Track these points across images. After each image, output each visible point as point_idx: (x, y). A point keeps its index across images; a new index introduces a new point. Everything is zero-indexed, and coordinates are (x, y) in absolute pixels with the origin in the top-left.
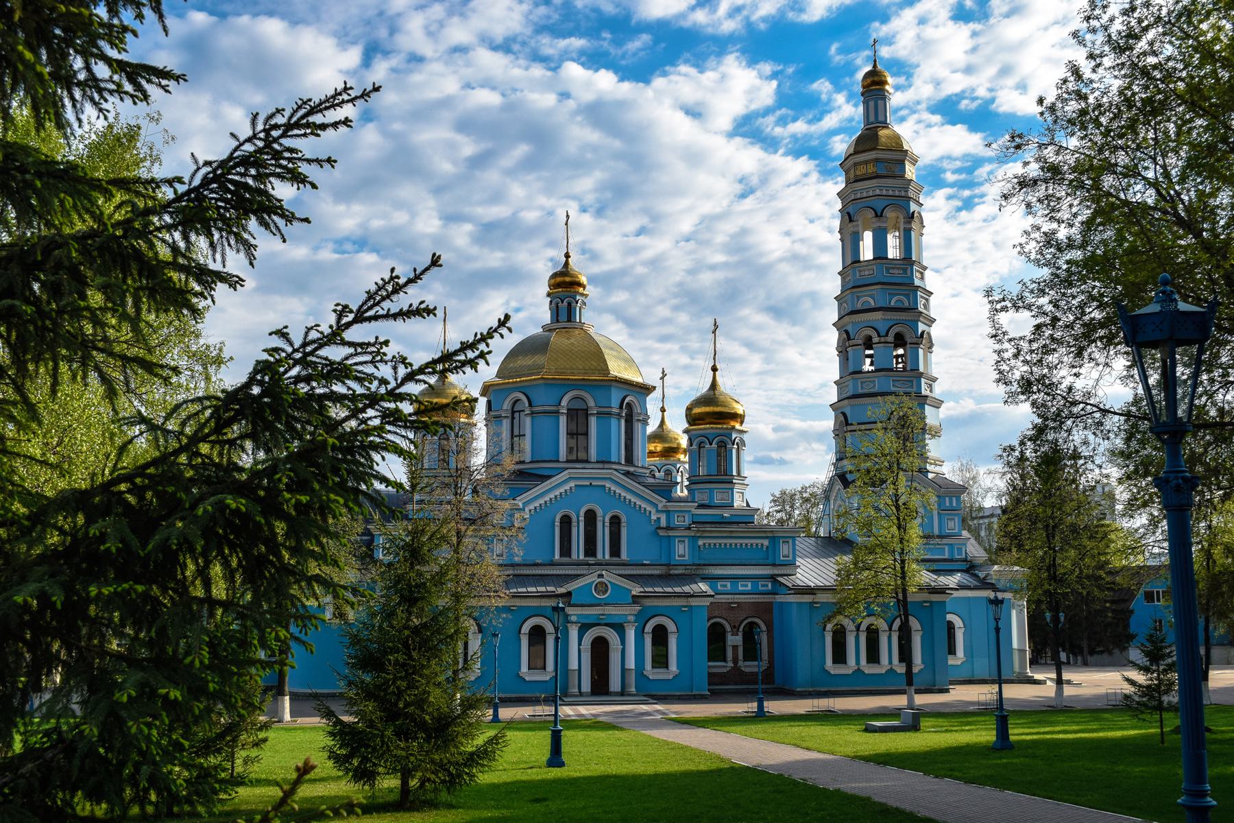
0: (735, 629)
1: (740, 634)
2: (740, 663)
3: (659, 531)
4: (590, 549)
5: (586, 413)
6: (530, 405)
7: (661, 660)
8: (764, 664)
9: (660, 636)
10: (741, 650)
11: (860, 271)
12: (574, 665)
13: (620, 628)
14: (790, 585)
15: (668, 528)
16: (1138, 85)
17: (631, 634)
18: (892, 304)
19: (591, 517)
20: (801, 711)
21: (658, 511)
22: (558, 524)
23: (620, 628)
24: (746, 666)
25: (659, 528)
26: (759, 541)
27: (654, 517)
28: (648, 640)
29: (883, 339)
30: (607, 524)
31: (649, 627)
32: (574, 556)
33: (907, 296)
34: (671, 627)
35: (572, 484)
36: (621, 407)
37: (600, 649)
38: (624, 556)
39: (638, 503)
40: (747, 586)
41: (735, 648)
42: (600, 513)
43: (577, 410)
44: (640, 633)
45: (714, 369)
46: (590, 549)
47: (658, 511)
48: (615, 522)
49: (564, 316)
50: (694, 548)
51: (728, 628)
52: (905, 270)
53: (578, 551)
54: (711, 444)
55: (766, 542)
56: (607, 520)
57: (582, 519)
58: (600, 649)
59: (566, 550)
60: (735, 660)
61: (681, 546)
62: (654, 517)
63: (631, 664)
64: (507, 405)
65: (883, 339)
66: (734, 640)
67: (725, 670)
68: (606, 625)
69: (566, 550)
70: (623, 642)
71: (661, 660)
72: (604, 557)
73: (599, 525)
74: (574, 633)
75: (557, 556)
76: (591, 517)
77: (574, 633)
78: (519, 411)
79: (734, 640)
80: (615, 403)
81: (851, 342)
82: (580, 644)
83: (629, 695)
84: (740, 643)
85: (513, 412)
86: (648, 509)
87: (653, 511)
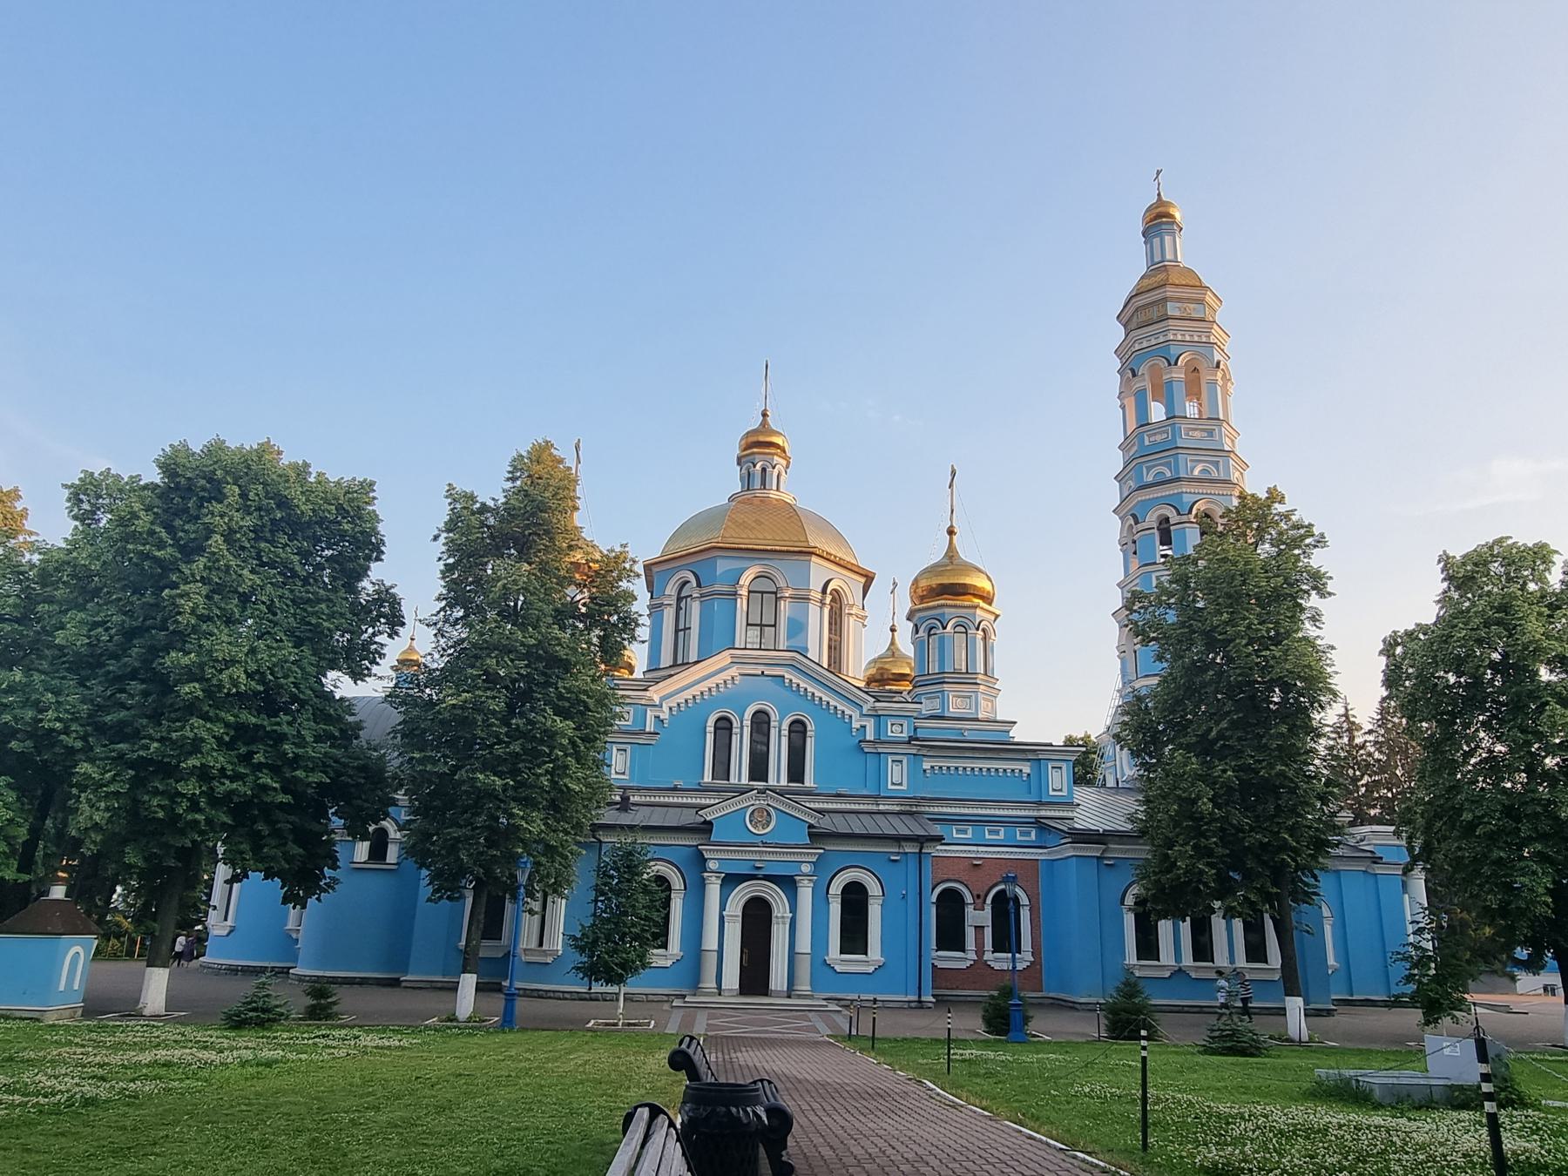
0: (979, 899)
1: (988, 909)
2: (988, 956)
3: (863, 745)
4: (759, 769)
5: (776, 595)
6: (699, 585)
7: (854, 938)
8: (1025, 958)
9: (855, 899)
10: (988, 933)
11: (1149, 436)
12: (711, 942)
13: (788, 883)
14: (1066, 829)
15: (877, 742)
16: (1179, 869)
17: (805, 893)
18: (1196, 472)
19: (761, 722)
20: (1225, 934)
21: (862, 715)
22: (710, 729)
23: (788, 883)
24: (996, 960)
25: (865, 741)
26: (1017, 766)
27: (856, 725)
28: (835, 909)
29: (1185, 518)
30: (785, 733)
31: (836, 888)
32: (733, 780)
33: (1216, 464)
34: (874, 888)
35: (734, 671)
36: (824, 591)
37: (757, 918)
38: (809, 782)
39: (832, 703)
40: (997, 833)
41: (979, 929)
42: (775, 716)
43: (762, 593)
44: (821, 897)
45: (951, 532)
46: (759, 769)
47: (862, 715)
48: (798, 730)
49: (757, 483)
50: (916, 773)
51: (969, 899)
52: (1211, 433)
53: (740, 773)
54: (944, 628)
55: (1026, 769)
56: (785, 726)
57: (747, 723)
58: (757, 918)
59: (722, 767)
60: (980, 951)
61: (897, 768)
62: (856, 725)
63: (804, 944)
64: (671, 589)
65: (1185, 518)
66: (978, 917)
67: (963, 965)
68: (767, 878)
69: (722, 767)
70: (793, 909)
71: (854, 938)
72: (740, 780)
73: (773, 733)
74: (714, 890)
75: (708, 778)
76: (761, 722)
77: (714, 890)
78: (686, 597)
79: (978, 917)
80: (816, 585)
81: (1140, 527)
82: (723, 907)
83: (799, 997)
84: (969, 910)
85: (679, 599)
86: (847, 712)
87: (856, 715)
